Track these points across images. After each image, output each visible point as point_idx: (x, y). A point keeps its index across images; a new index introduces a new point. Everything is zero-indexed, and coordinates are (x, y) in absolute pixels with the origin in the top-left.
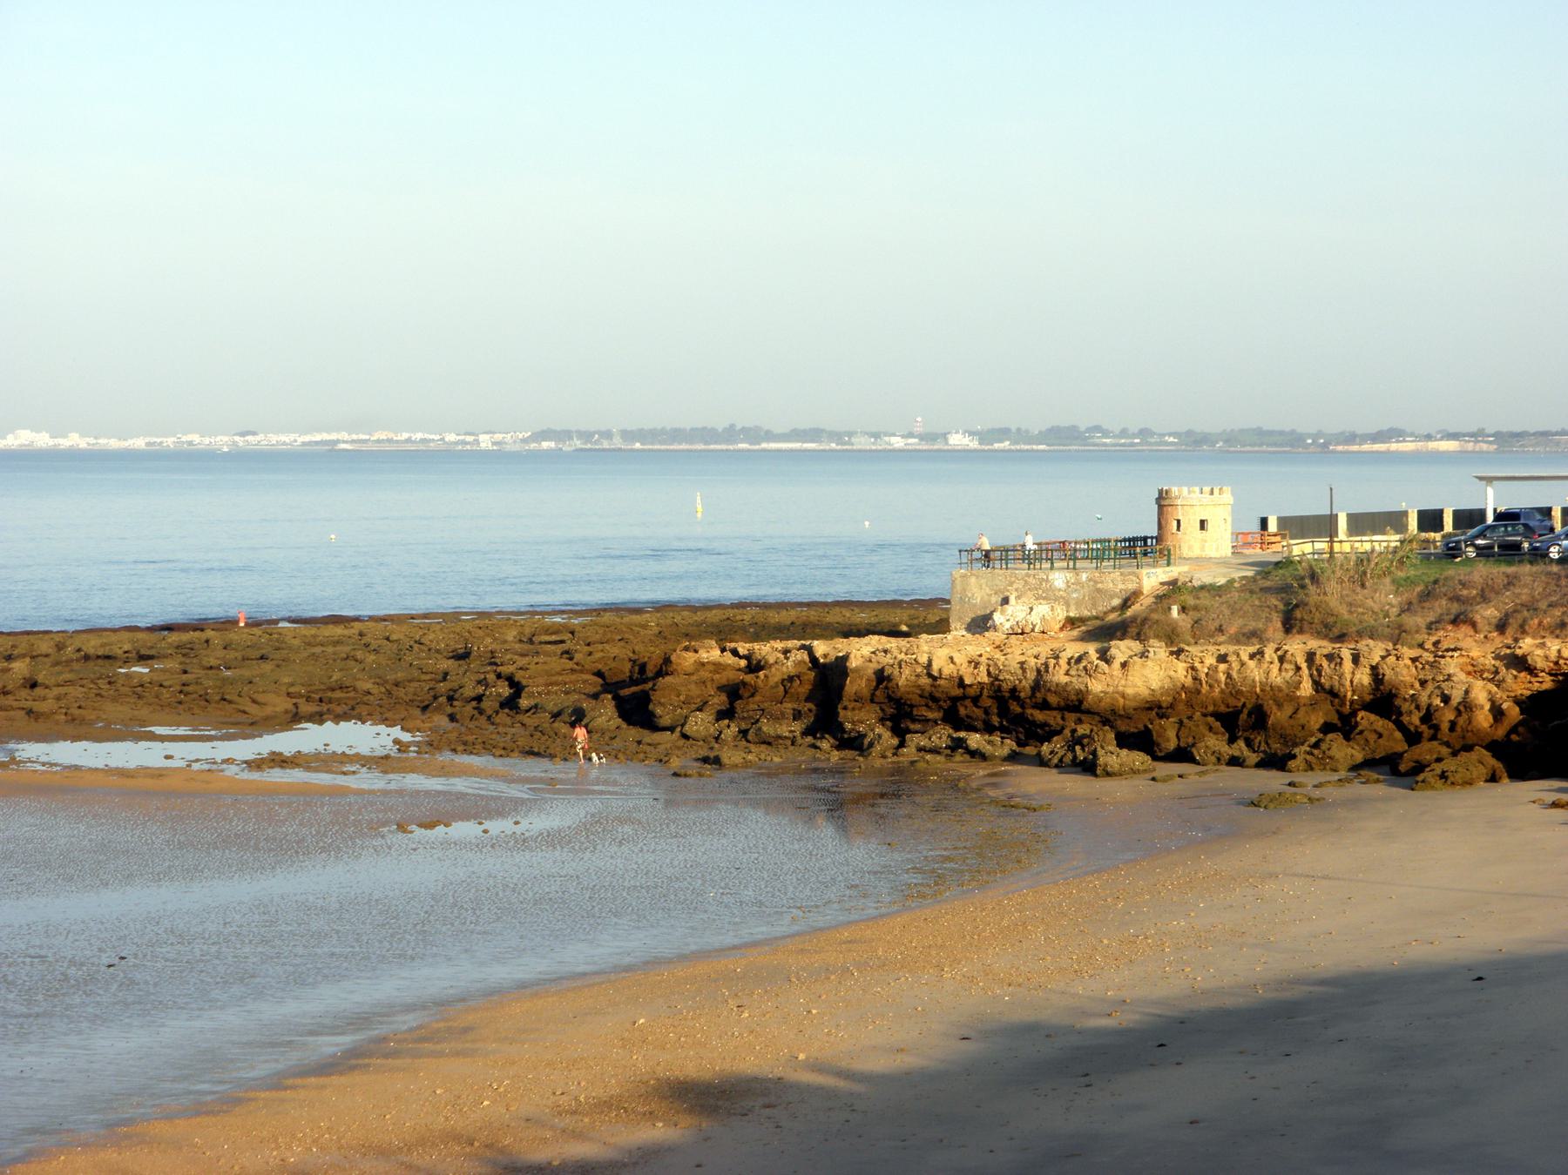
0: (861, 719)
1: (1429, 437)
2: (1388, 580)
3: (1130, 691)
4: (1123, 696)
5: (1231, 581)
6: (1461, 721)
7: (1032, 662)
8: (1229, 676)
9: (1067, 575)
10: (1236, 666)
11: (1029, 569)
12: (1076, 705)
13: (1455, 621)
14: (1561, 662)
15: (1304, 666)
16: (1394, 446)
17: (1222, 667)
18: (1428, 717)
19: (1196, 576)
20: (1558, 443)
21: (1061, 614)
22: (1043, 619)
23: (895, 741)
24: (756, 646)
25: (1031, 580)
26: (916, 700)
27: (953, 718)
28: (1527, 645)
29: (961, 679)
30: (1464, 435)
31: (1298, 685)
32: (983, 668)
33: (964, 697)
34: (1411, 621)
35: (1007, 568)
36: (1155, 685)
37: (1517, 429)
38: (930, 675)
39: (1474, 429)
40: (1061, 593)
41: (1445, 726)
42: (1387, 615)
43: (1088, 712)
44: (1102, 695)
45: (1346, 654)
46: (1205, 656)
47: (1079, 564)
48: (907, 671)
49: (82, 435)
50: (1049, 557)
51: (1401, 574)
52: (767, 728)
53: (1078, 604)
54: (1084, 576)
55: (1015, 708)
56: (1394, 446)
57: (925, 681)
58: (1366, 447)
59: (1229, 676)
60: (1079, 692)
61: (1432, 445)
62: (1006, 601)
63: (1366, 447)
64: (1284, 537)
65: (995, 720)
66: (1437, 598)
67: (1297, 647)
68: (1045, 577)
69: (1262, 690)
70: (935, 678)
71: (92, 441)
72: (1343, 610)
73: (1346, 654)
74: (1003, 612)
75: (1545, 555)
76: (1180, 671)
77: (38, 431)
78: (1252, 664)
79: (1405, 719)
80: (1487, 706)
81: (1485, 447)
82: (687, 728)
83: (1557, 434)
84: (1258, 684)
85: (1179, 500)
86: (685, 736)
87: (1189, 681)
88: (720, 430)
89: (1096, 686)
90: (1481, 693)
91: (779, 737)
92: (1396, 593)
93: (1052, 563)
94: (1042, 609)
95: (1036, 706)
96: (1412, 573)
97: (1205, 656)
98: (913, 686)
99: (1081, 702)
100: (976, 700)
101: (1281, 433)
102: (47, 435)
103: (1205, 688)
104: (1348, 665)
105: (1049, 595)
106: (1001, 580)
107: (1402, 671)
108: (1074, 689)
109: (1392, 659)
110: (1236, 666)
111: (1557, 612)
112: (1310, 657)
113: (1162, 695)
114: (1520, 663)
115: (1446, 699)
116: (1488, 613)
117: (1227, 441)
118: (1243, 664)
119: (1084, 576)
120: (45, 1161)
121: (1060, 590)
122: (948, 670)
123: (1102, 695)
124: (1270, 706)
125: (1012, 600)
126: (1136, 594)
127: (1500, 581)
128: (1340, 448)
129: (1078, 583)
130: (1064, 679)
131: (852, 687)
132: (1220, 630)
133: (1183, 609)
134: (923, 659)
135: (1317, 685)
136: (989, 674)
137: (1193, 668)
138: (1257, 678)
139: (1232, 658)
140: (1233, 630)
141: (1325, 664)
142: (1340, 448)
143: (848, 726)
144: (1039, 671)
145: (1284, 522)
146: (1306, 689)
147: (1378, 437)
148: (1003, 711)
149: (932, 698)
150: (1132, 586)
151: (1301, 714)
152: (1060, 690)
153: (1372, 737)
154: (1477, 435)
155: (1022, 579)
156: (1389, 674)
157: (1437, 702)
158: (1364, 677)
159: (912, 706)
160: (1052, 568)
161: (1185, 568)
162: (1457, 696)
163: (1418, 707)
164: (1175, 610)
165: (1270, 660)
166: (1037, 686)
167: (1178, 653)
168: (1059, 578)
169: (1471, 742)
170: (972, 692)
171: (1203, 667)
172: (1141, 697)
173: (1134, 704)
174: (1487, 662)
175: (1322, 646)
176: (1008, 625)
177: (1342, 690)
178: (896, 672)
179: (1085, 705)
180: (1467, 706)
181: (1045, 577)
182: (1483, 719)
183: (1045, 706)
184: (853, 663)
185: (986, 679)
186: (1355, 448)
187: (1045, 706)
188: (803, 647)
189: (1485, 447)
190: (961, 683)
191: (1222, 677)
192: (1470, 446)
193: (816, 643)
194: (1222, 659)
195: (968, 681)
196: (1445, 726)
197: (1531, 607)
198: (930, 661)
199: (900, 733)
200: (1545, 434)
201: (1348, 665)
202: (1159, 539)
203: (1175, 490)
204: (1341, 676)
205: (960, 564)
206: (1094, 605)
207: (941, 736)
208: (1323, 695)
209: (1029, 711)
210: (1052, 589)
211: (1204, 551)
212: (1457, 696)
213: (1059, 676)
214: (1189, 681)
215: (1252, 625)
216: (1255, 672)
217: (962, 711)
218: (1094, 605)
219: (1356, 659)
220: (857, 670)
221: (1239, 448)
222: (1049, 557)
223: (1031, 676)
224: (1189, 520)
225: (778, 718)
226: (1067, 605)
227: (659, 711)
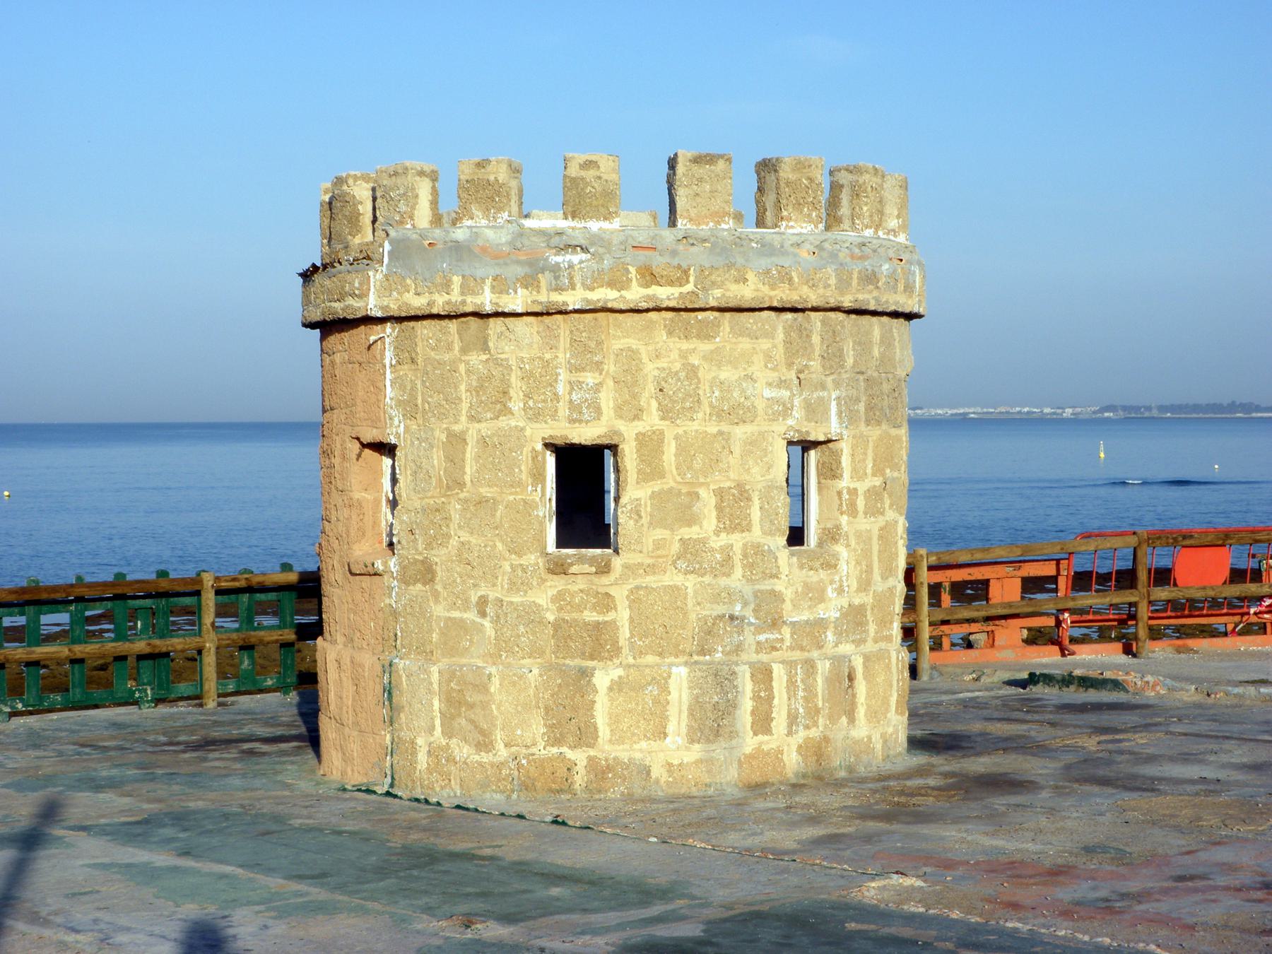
211: (586, 736)
224: (457, 440)
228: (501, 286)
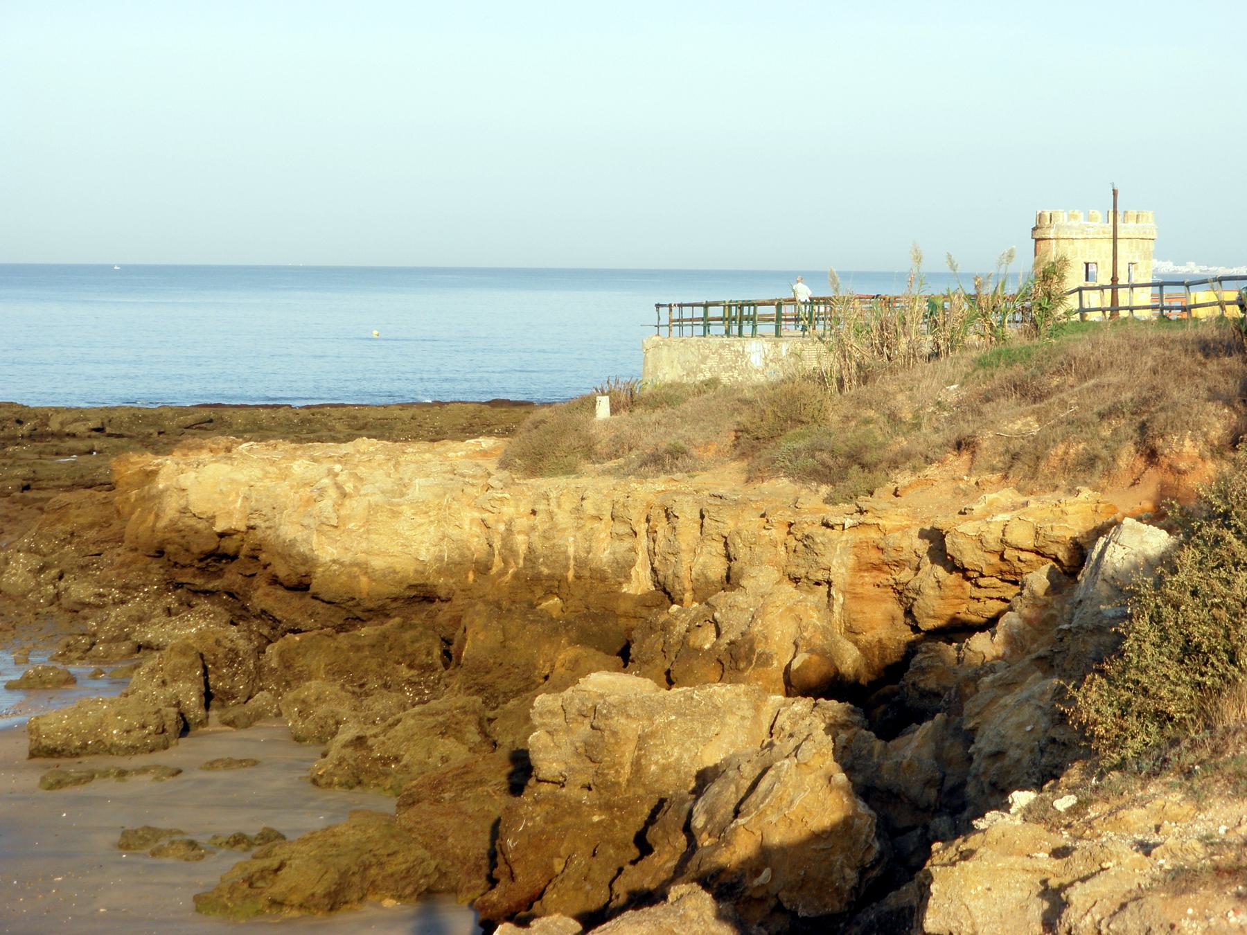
3: (378, 563)
9: (765, 346)
11: (728, 333)
14: (1009, 554)
25: (725, 353)
35: (753, 335)
36: (424, 556)
40: (759, 376)
44: (335, 567)
49: (1197, 264)
50: (772, 310)
68: (741, 349)
69: (578, 577)
71: (1205, 268)
77: (1165, 260)
84: (572, 562)
85: (1052, 231)
93: (754, 327)
98: (171, 531)
102: (1171, 264)
103: (497, 564)
106: (693, 353)
108: (299, 553)
113: (439, 572)
120: (1228, 884)
121: (757, 371)
123: (335, 567)
138: (571, 551)
155: (717, 351)
165: (593, 512)
171: (497, 521)
172: (398, 577)
174: (905, 543)
177: (677, 587)
181: (741, 349)
203: (1062, 218)
205: (658, 326)
222: (772, 310)
228: (1077, 233)
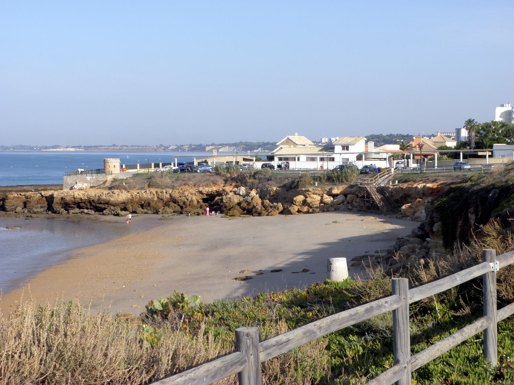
0: (56, 207)
1: (67, 147)
2: (167, 177)
3: (119, 200)
4: (118, 201)
5: (127, 178)
6: (191, 203)
7: (97, 194)
8: (140, 196)
10: (141, 194)
12: (108, 203)
13: (184, 185)
15: (155, 194)
16: (58, 150)
17: (138, 194)
18: (184, 203)
19: (119, 177)
20: (100, 149)
21: (89, 185)
22: (86, 186)
23: (66, 212)
24: (26, 193)
25: (82, 178)
26: (71, 203)
27: (79, 207)
28: (201, 189)
29: (81, 198)
30: (76, 147)
31: (154, 198)
32: (86, 196)
33: (82, 202)
34: (175, 184)
36: (124, 199)
37: (90, 145)
38: (74, 198)
39: (78, 145)
41: (188, 205)
42: (169, 184)
43: (110, 204)
45: (164, 191)
46: (135, 193)
47: (93, 175)
48: (68, 197)
51: (169, 176)
52: (35, 210)
53: (93, 183)
54: (94, 177)
55: (94, 204)
56: (58, 150)
57: (73, 199)
58: (51, 150)
59: (140, 196)
60: (108, 200)
61: (68, 149)
62: (76, 183)
63: (51, 150)
64: (127, 169)
65: (89, 207)
66: (179, 180)
67: (154, 190)
70: (75, 198)
72: (160, 183)
73: (164, 191)
74: (76, 185)
75: (197, 172)
76: (129, 196)
78: (144, 194)
79: (179, 204)
80: (196, 201)
81: (81, 150)
82: (16, 211)
83: (100, 146)
86: (16, 212)
87: (131, 198)
88: (453, 147)
89: (112, 199)
90: (194, 198)
91: (38, 212)
92: (170, 179)
94: (86, 184)
95: (98, 204)
96: (171, 175)
97: (135, 193)
99: (109, 202)
100: (84, 203)
101: (27, 146)
103: (134, 199)
104: (165, 194)
105: (86, 182)
107: (176, 194)
109: (174, 192)
110: (141, 194)
111: (206, 182)
112: (157, 192)
114: (201, 192)
115: (187, 200)
116: (191, 183)
117: (13, 148)
118: (142, 194)
119: (94, 177)
122: (78, 196)
124: (151, 202)
125: (78, 183)
126: (106, 181)
127: (192, 177)
128: (44, 150)
129: (93, 179)
130: (105, 198)
131: (55, 201)
132: (135, 187)
133: (125, 183)
134: (72, 194)
135: (158, 198)
136: (87, 197)
137: (132, 195)
139: (140, 193)
140: (137, 187)
141: (160, 194)
142: (44, 150)
143: (55, 209)
144: (99, 196)
145: (295, 160)
146: (156, 199)
147: (53, 147)
148: (91, 205)
149: (75, 203)
150: (105, 179)
151: (157, 203)
152: (104, 200)
153: (174, 207)
154: (79, 147)
156: (173, 195)
157: (186, 200)
158: (168, 196)
159: (69, 204)
160: (87, 176)
161: (114, 176)
162: (190, 199)
163: (182, 201)
164: (124, 183)
166: (99, 199)
167: (128, 192)
168: (89, 178)
169: (469, 176)
170: (83, 201)
173: (119, 202)
175: (159, 190)
176: (78, 188)
178: (66, 197)
179: (109, 203)
180: (192, 201)
182: (195, 202)
183: (101, 203)
184: (55, 196)
185: (87, 198)
186: (48, 150)
187: (101, 203)
188: (39, 193)
189: (81, 150)
190: (81, 199)
191: (138, 197)
192: (78, 150)
193: (42, 192)
194: (138, 193)
195: (83, 199)
196: (188, 205)
197: (200, 181)
198: (74, 195)
199: (67, 210)
200: (97, 146)
201: (165, 194)
202: (105, 169)
204: (163, 196)
206: (96, 183)
207: (77, 210)
208: (159, 200)
209: (97, 205)
210: (87, 180)
212: (190, 199)
213: (104, 197)
214: (131, 198)
215: (141, 186)
216: (145, 195)
217: (81, 205)
218: (96, 183)
219: (166, 192)
220: (56, 197)
221: (16, 150)
223: (97, 197)
225: (37, 208)
226: (90, 183)
227: (7, 207)
